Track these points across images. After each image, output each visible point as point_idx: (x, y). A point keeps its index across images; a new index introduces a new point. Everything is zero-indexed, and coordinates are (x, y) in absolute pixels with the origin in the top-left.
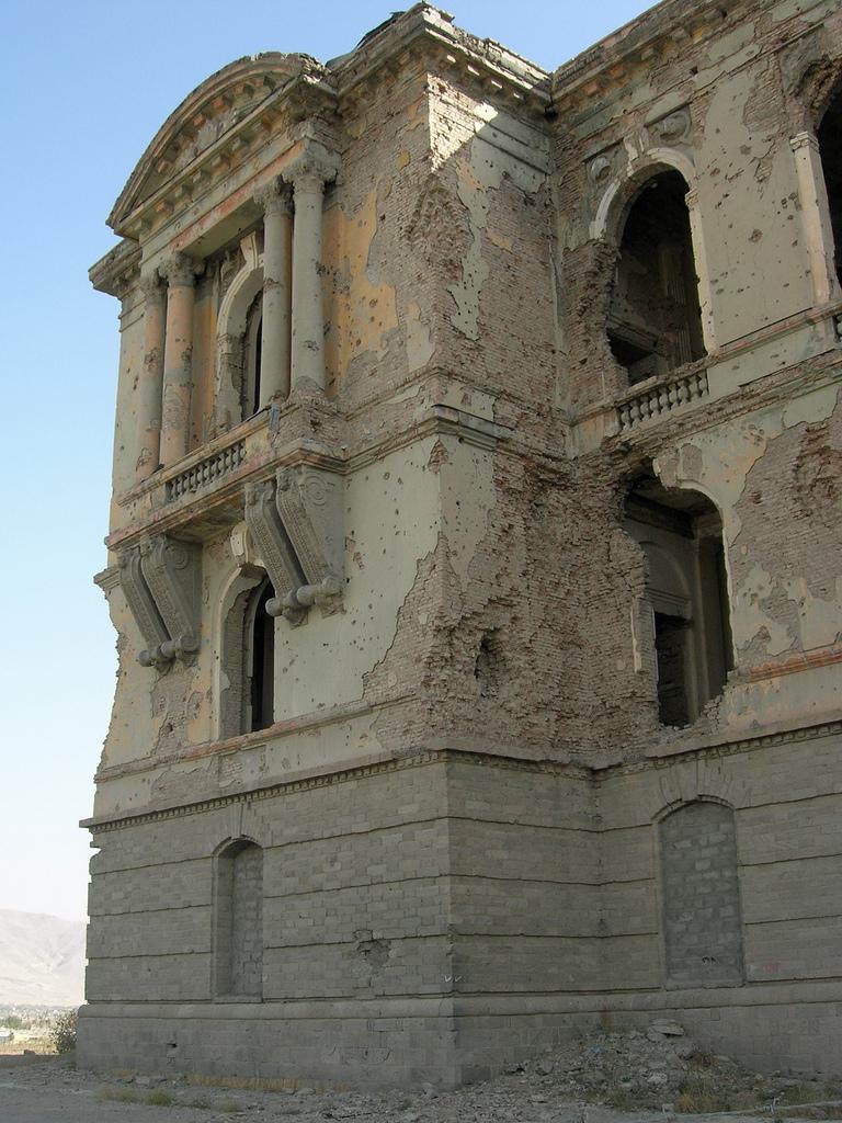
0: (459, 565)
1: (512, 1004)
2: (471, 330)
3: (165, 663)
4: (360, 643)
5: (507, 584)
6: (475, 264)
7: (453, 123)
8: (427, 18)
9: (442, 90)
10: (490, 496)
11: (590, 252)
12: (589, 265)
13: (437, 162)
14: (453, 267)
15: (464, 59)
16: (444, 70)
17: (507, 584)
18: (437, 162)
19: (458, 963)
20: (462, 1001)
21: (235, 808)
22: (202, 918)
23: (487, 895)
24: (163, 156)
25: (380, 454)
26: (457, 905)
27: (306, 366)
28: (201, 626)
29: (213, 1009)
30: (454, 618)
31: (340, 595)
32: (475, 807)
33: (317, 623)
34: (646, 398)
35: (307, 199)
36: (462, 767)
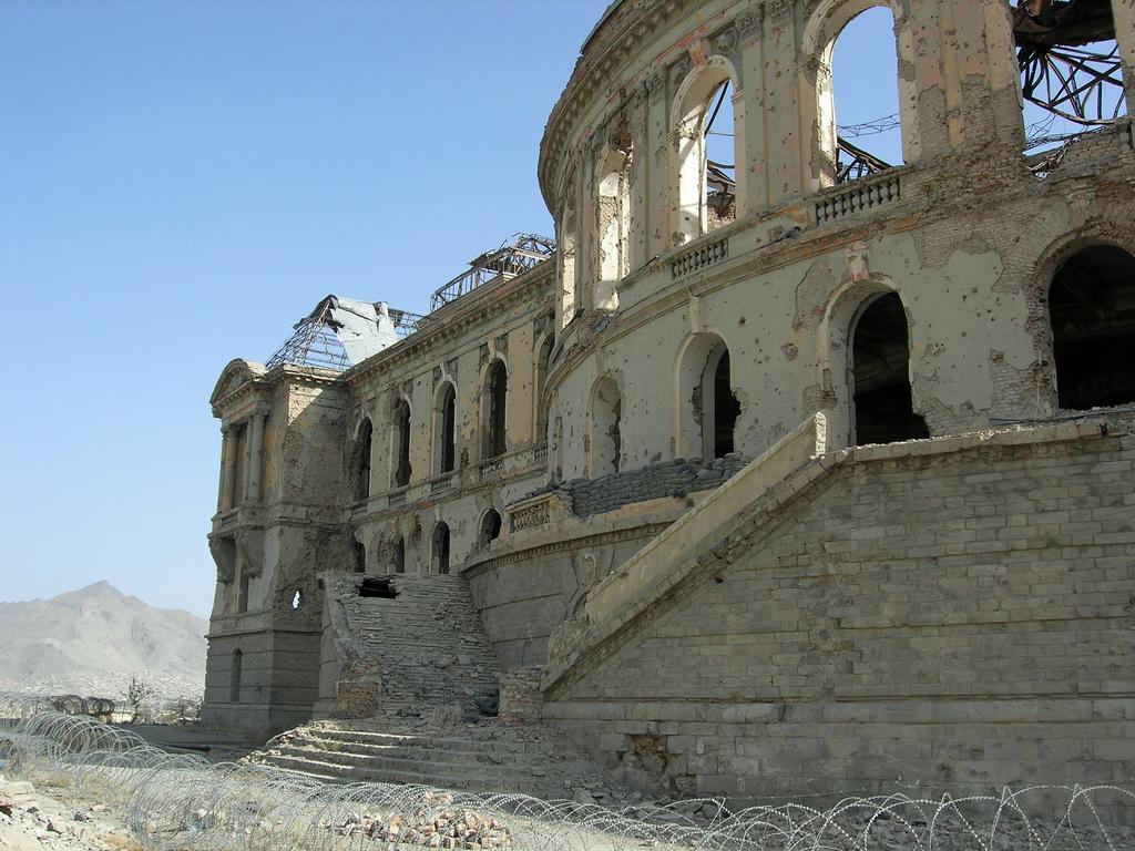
0: (285, 570)
1: (293, 708)
2: (299, 485)
3: (226, 582)
4: (761, 357)
5: (305, 573)
6: (304, 458)
7: (299, 401)
8: (285, 368)
9: (297, 389)
10: (300, 543)
11: (353, 445)
12: (352, 450)
13: (291, 421)
14: (293, 462)
15: (303, 378)
16: (297, 382)
17: (305, 573)
18: (291, 421)
19: (273, 695)
20: (273, 706)
21: (236, 639)
22: (229, 674)
23: (699, 655)
24: (225, 381)
25: (270, 527)
26: (275, 676)
27: (253, 492)
28: (263, 555)
29: (229, 706)
30: (282, 587)
31: (260, 572)
32: (283, 647)
33: (257, 579)
34: (886, 184)
35: (257, 424)
36: (281, 635)
